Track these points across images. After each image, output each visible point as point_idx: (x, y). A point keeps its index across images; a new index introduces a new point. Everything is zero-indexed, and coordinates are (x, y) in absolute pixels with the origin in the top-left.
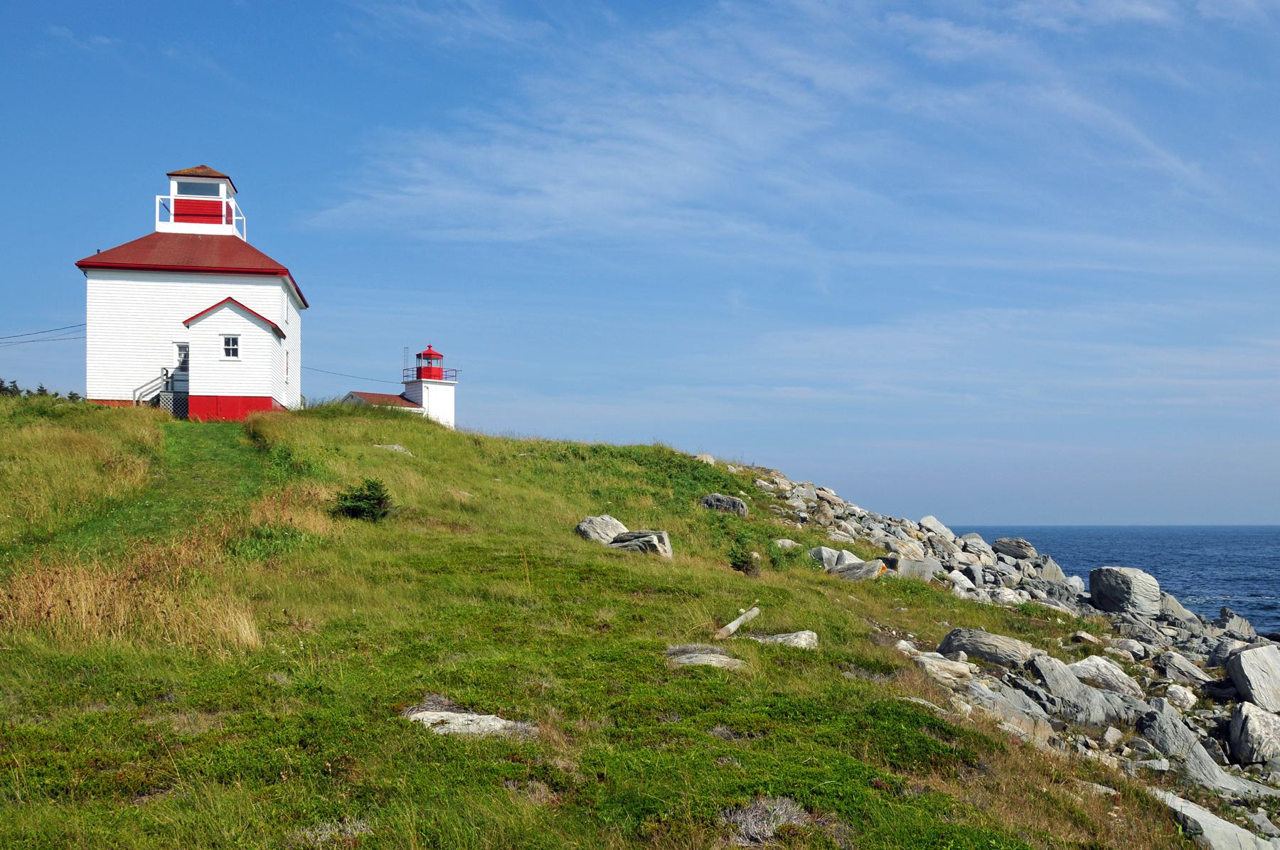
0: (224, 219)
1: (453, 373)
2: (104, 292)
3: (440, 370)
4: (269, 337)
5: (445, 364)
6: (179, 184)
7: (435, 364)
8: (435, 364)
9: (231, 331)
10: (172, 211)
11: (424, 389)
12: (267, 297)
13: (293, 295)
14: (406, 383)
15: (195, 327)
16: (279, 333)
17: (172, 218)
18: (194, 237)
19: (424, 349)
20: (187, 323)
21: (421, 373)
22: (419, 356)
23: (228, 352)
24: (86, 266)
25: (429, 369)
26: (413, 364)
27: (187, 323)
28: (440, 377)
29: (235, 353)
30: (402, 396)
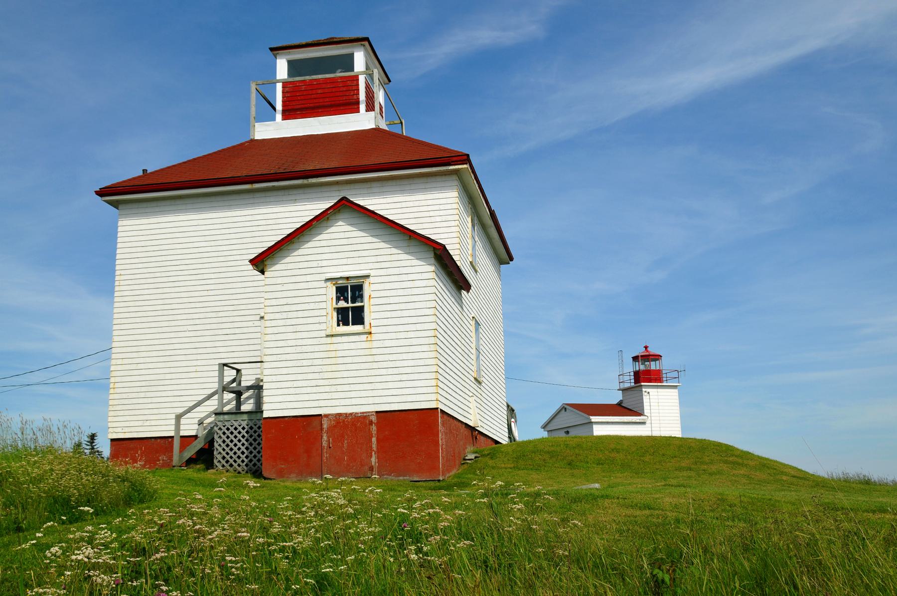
0: (362, 107)
1: (675, 374)
2: (147, 238)
3: (659, 372)
4: (425, 271)
5: (664, 365)
6: (291, 63)
7: (653, 366)
8: (653, 366)
9: (348, 269)
10: (279, 106)
11: (646, 399)
12: (435, 211)
13: (483, 227)
14: (624, 390)
15: (278, 270)
16: (458, 282)
17: (279, 116)
18: (283, 102)
19: (640, 351)
20: (260, 262)
21: (639, 377)
22: (635, 359)
23: (343, 317)
24: (127, 194)
25: (648, 372)
26: (630, 368)
27: (260, 262)
28: (659, 380)
29: (358, 318)
30: (620, 404)
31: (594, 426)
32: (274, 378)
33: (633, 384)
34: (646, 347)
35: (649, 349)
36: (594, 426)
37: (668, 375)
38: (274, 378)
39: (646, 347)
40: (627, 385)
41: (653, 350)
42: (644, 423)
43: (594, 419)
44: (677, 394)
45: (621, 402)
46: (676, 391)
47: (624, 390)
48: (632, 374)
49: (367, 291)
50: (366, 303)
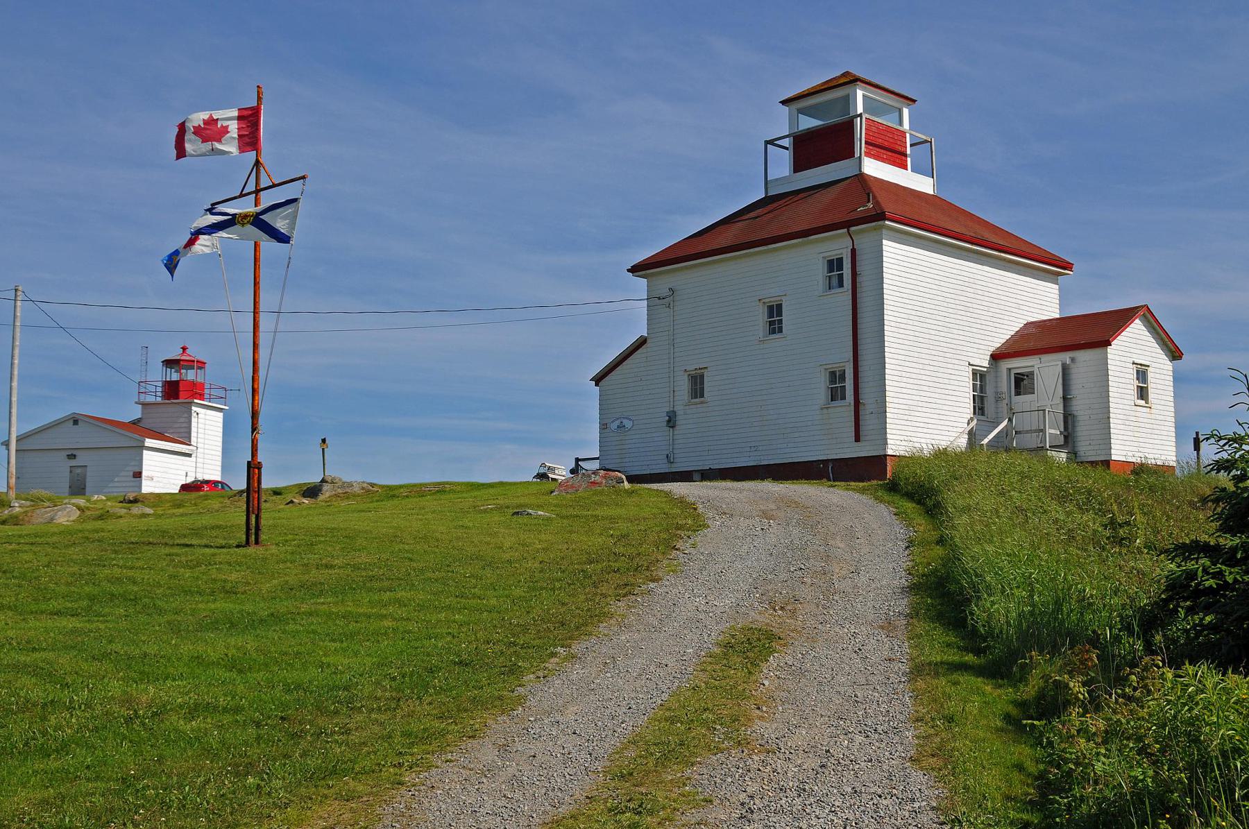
1: (222, 393)
7: (190, 375)
8: (190, 375)
19: (175, 354)
21: (172, 390)
22: (169, 363)
26: (158, 375)
30: (135, 423)
31: (145, 452)
32: (896, 400)
33: (159, 399)
34: (184, 349)
35: (188, 351)
36: (145, 452)
37: (213, 392)
38: (896, 400)
39: (184, 349)
40: (150, 399)
41: (195, 353)
42: (189, 455)
43: (149, 442)
44: (221, 420)
45: (139, 420)
46: (221, 415)
47: (145, 405)
48: (160, 384)
49: (1150, 375)
50: (784, 318)
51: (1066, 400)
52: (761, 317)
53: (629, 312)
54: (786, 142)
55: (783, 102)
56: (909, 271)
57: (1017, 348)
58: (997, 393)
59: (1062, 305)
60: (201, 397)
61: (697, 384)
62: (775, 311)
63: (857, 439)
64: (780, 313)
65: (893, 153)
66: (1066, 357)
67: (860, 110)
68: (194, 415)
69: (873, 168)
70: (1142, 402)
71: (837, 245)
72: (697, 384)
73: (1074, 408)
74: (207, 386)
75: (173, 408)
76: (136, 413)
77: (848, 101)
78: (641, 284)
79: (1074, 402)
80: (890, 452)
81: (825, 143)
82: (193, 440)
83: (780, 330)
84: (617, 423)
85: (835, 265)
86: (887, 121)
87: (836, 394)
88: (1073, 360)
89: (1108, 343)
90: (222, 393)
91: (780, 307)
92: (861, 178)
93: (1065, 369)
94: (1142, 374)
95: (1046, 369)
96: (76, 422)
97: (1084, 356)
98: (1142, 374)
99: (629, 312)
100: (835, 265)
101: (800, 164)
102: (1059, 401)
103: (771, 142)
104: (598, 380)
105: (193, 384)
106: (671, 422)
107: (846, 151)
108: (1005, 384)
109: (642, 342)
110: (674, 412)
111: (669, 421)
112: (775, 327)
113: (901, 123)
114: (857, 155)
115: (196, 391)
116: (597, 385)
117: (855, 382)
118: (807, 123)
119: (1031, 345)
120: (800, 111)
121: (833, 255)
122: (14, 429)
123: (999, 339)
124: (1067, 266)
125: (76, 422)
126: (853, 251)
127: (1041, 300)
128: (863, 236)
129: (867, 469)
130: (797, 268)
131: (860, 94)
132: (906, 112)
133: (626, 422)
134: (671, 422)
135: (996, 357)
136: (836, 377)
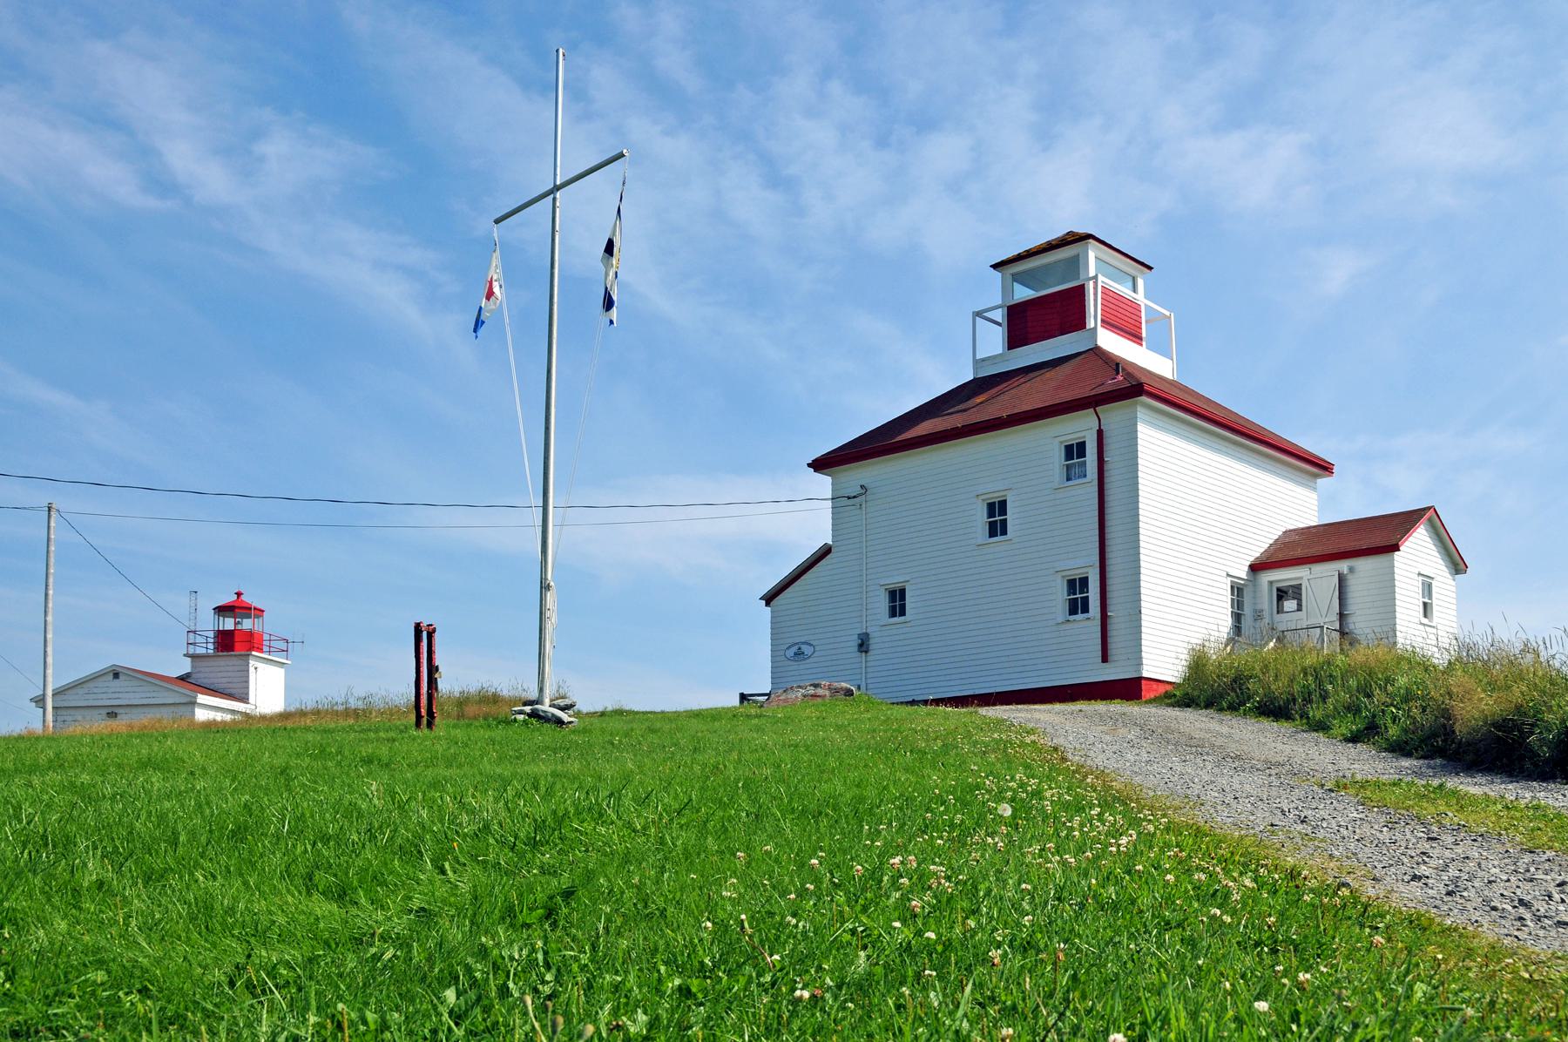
1: (283, 645)
7: (247, 624)
8: (247, 624)
21: (225, 641)
22: (222, 610)
26: (209, 624)
30: (183, 679)
34: (239, 594)
35: (243, 598)
39: (239, 594)
40: (200, 651)
43: (202, 699)
47: (194, 657)
48: (211, 634)
50: (1009, 517)
51: (1342, 616)
52: (981, 518)
53: (804, 516)
54: (999, 315)
55: (995, 266)
56: (1163, 456)
57: (1281, 556)
58: (1255, 611)
59: (1321, 509)
60: (261, 650)
61: (897, 601)
62: (997, 509)
63: (1105, 659)
64: (1003, 511)
65: (1126, 322)
66: (1343, 566)
67: (1092, 273)
68: (252, 670)
69: (1110, 342)
70: (1425, 621)
71: (1080, 426)
72: (897, 601)
73: (1352, 626)
74: (266, 637)
75: (227, 663)
76: (185, 667)
77: (1076, 264)
78: (823, 484)
79: (1351, 620)
80: (1145, 674)
81: (1047, 312)
82: (251, 700)
83: (1004, 532)
84: (794, 649)
85: (1075, 451)
86: (1124, 290)
87: (1077, 606)
88: (1351, 570)
89: (1396, 548)
90: (283, 645)
91: (1003, 504)
92: (1097, 351)
93: (1342, 579)
94: (1428, 589)
95: (1318, 580)
96: (116, 675)
97: (1364, 565)
98: (1428, 589)
99: (804, 516)
100: (1075, 451)
101: (1016, 339)
102: (1335, 617)
103: (978, 314)
104: (769, 599)
105: (250, 634)
106: (864, 645)
107: (1075, 320)
108: (1266, 600)
109: (825, 552)
110: (867, 635)
111: (861, 645)
112: (997, 529)
113: (1135, 290)
114: (1091, 323)
115: (252, 642)
116: (768, 604)
117: (1099, 592)
118: (1023, 293)
119: (1299, 553)
120: (1017, 278)
121: (1073, 439)
122: (50, 679)
123: (1256, 551)
124: (1325, 468)
125: (116, 675)
126: (1100, 433)
127: (1298, 506)
128: (1113, 415)
129: (1130, 689)
130: (1024, 459)
131: (1092, 255)
132: (1140, 282)
133: (804, 647)
134: (864, 645)
135: (1255, 568)
136: (1077, 585)
